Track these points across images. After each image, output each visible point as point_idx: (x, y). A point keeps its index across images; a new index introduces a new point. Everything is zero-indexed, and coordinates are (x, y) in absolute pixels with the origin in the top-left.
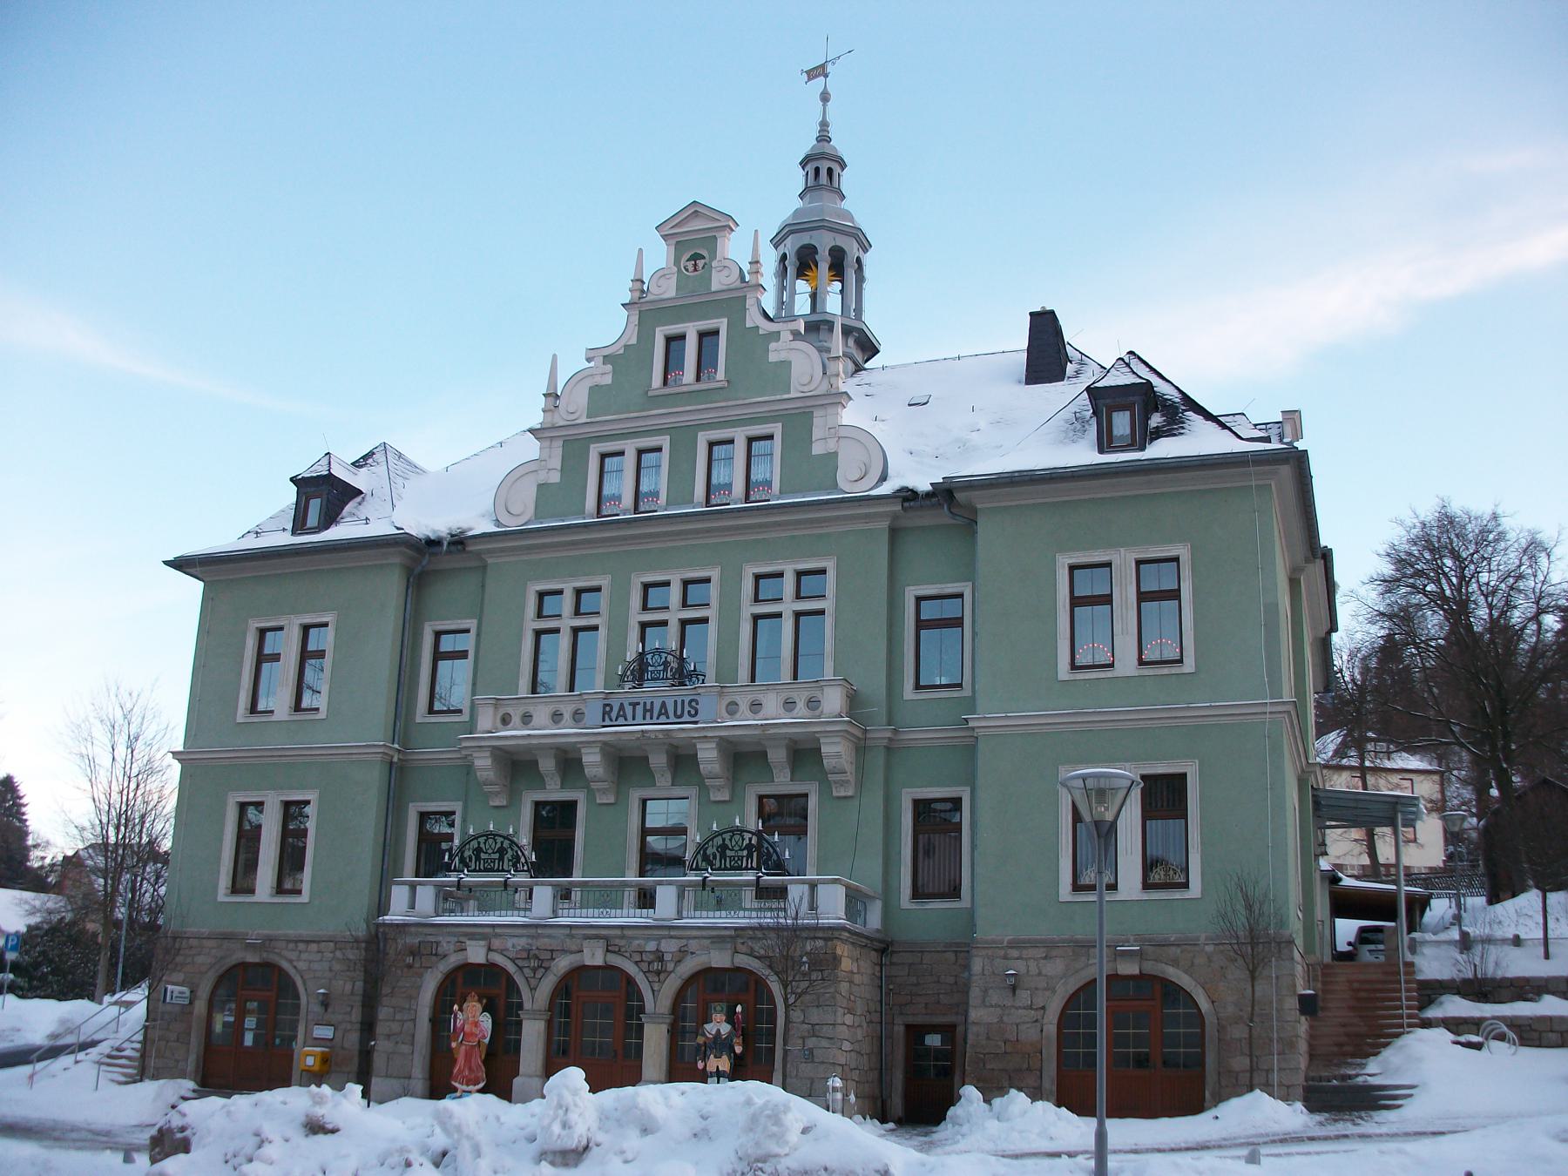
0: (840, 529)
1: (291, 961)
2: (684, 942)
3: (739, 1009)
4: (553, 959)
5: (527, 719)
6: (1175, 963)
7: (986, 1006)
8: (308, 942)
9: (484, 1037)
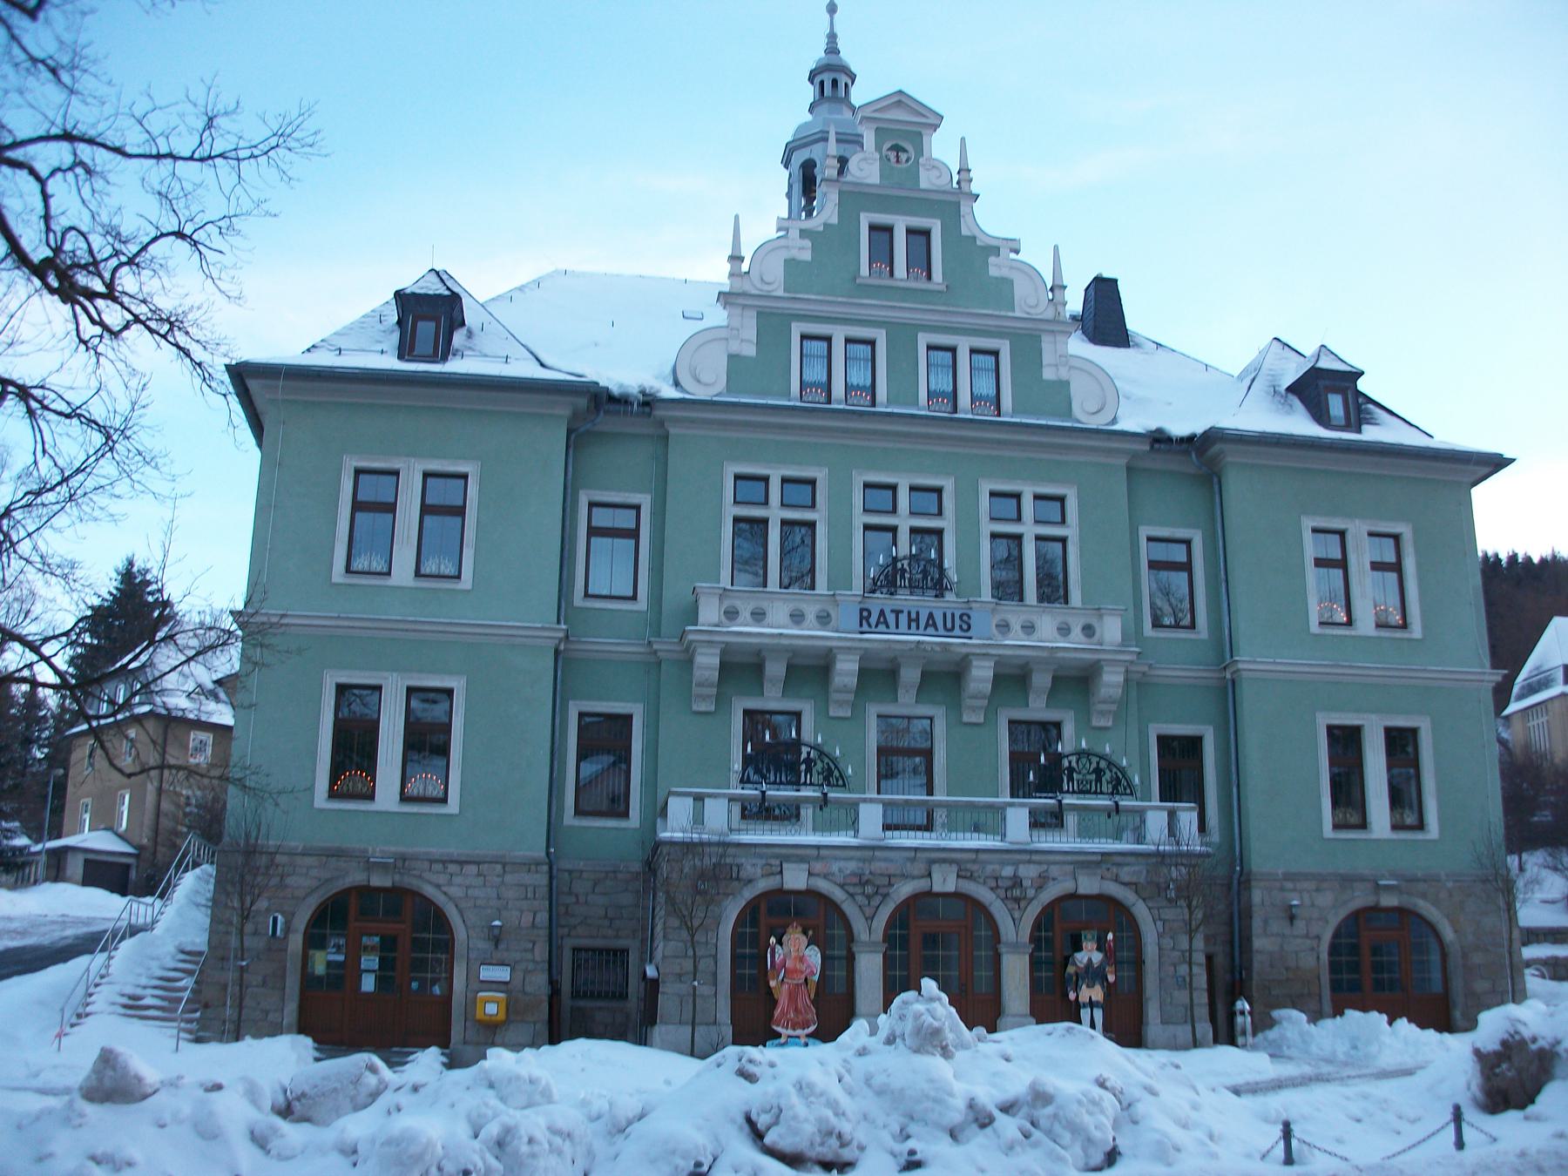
0: (1082, 459)
1: (438, 886)
2: (1045, 867)
3: (1110, 936)
4: (890, 885)
5: (759, 616)
6: (1424, 896)
8: (462, 863)
9: (813, 973)
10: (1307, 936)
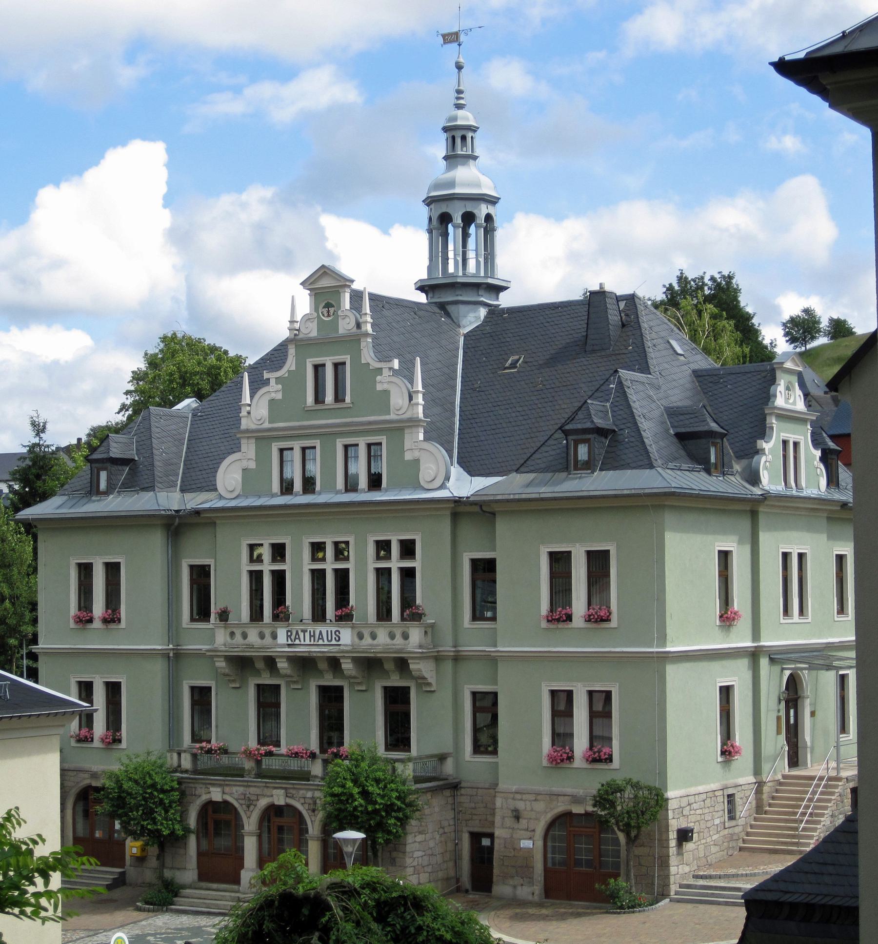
4: (258, 800)
7: (504, 828)
10: (527, 830)
